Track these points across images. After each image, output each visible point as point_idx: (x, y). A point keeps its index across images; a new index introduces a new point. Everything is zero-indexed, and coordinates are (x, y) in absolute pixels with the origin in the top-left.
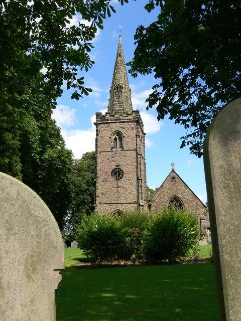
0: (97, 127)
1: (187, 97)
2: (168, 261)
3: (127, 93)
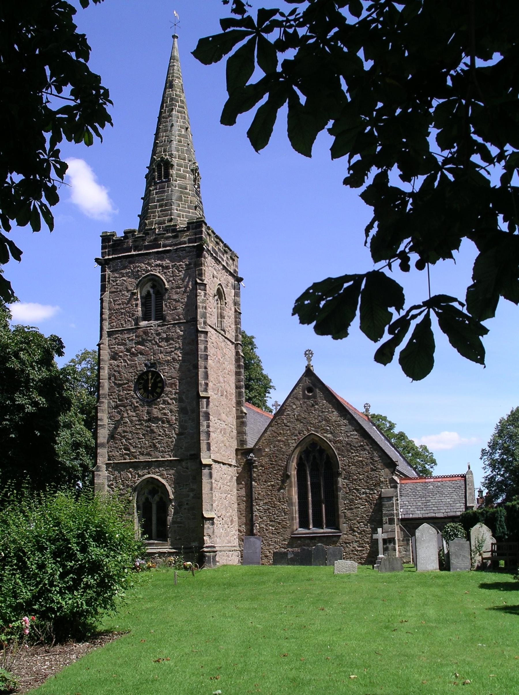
0: (103, 270)
1: (323, 303)
2: (368, 65)
3: (184, 177)
